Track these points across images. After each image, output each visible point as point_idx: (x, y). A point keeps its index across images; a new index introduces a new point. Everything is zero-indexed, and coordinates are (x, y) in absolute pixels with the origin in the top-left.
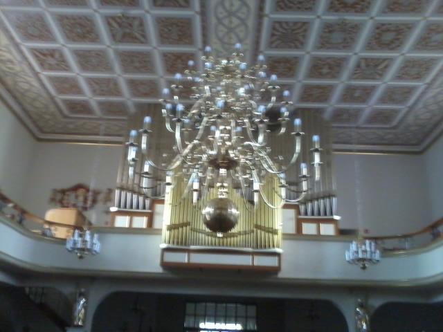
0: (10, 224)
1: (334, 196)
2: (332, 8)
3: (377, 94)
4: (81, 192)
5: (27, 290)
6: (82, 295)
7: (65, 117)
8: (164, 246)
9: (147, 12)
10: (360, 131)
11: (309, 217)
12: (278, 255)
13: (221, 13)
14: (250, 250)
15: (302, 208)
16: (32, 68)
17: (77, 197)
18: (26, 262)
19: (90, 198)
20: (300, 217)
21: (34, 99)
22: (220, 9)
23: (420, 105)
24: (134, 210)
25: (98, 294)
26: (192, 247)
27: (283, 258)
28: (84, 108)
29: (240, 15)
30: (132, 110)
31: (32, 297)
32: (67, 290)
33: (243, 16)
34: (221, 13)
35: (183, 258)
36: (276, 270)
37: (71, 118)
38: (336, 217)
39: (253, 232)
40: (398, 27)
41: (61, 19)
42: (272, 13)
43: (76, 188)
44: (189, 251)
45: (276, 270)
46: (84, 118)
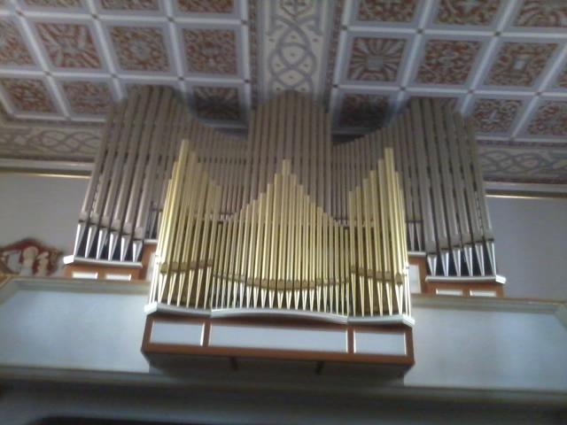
1: (491, 240)
2: (442, 17)
4: (29, 253)
8: (152, 307)
9: (171, 20)
10: (514, 151)
11: (447, 277)
13: (278, 65)
14: (343, 318)
15: (432, 263)
17: (21, 260)
22: (276, 59)
24: (109, 261)
26: (216, 312)
28: (30, 96)
29: (301, 67)
30: (120, 94)
33: (307, 70)
34: (278, 65)
35: (190, 335)
36: (403, 364)
37: (20, 121)
38: (500, 279)
40: (510, 82)
41: (42, 28)
42: (352, 23)
43: (26, 244)
44: (208, 321)
45: (403, 364)
46: (40, 122)
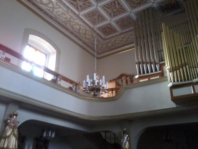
0: (69, 92)
4: (123, 78)
5: (103, 134)
6: (125, 132)
7: (104, 39)
8: (170, 85)
16: (75, 14)
18: (84, 115)
19: (129, 80)
21: (85, 34)
24: (150, 73)
25: (136, 131)
31: (108, 140)
32: (116, 131)
35: (189, 91)
37: (107, 39)
46: (113, 37)
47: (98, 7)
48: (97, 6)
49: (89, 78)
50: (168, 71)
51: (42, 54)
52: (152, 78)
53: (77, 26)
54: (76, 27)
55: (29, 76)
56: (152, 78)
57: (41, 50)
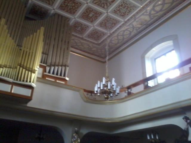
1: (68, 66)
3: (101, 19)
10: (82, 41)
12: (31, 87)
14: (11, 80)
20: (45, 73)
23: (116, 34)
24: (59, 76)
27: (35, 90)
36: (28, 99)
38: (67, 79)
39: (16, 68)
45: (28, 99)
47: (106, 12)
48: (107, 13)
49: (44, 35)
50: (37, 72)
51: (161, 57)
52: (57, 81)
53: (126, 32)
54: (127, 33)
55: (169, 83)
56: (57, 81)
57: (158, 56)
